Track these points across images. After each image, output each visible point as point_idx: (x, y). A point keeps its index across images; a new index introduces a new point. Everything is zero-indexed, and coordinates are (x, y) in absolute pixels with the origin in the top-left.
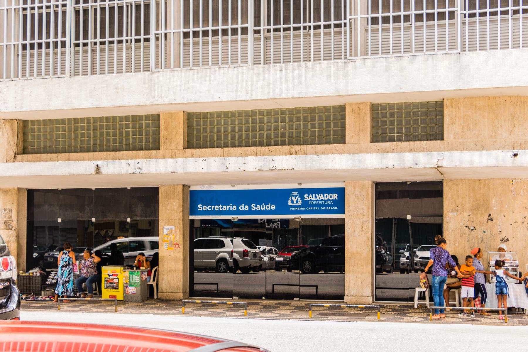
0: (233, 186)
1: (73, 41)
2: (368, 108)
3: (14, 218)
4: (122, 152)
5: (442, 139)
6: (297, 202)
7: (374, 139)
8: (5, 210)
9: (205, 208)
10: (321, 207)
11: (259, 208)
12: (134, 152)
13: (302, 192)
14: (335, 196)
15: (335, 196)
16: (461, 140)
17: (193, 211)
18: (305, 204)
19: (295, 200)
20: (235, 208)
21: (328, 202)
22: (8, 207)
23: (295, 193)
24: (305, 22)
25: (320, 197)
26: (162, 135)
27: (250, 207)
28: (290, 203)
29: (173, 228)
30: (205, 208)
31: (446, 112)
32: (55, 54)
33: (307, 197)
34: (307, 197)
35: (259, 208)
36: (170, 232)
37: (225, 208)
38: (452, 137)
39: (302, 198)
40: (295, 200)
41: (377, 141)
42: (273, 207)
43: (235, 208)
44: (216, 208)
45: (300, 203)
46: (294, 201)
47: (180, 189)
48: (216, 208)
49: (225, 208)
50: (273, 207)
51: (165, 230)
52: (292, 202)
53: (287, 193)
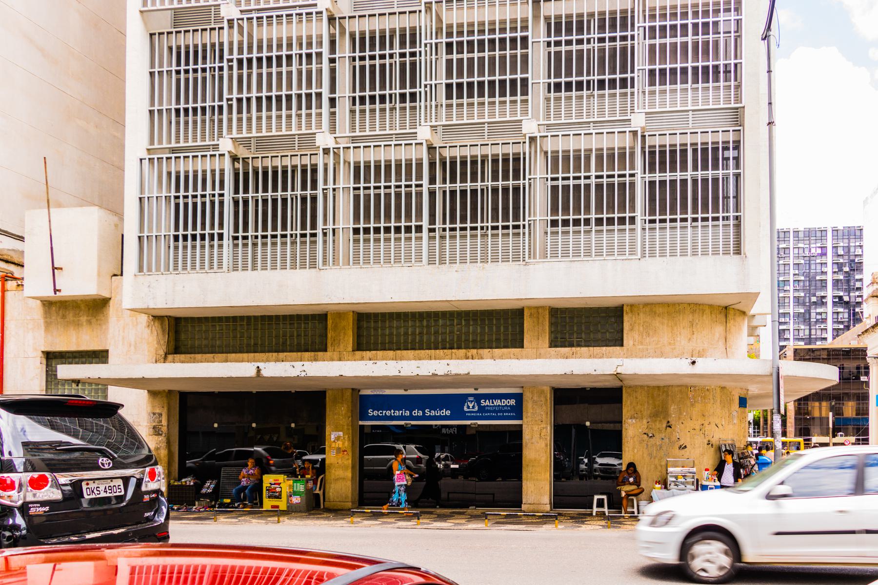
0: (406, 390)
1: (232, 233)
2: (547, 312)
3: (164, 422)
4: (285, 354)
5: (622, 345)
6: (473, 407)
7: (553, 344)
8: (154, 414)
9: (375, 413)
10: (498, 413)
11: (433, 413)
12: (299, 354)
13: (478, 398)
14: (512, 402)
15: (512, 402)
16: (641, 347)
17: (364, 416)
18: (482, 409)
19: (471, 406)
20: (408, 413)
21: (506, 408)
22: (158, 411)
23: (471, 399)
24: (482, 221)
25: (497, 402)
26: (329, 336)
27: (424, 413)
28: (465, 409)
29: (341, 434)
30: (375, 413)
31: (626, 318)
32: (212, 246)
33: (485, 403)
34: (485, 403)
35: (433, 413)
36: (338, 438)
37: (397, 413)
38: (631, 343)
39: (479, 404)
40: (471, 406)
41: (556, 346)
42: (448, 413)
43: (408, 413)
44: (388, 413)
45: (476, 408)
46: (470, 406)
47: (348, 394)
48: (388, 413)
49: (397, 413)
50: (448, 413)
51: (332, 436)
52: (468, 407)
53: (464, 398)
